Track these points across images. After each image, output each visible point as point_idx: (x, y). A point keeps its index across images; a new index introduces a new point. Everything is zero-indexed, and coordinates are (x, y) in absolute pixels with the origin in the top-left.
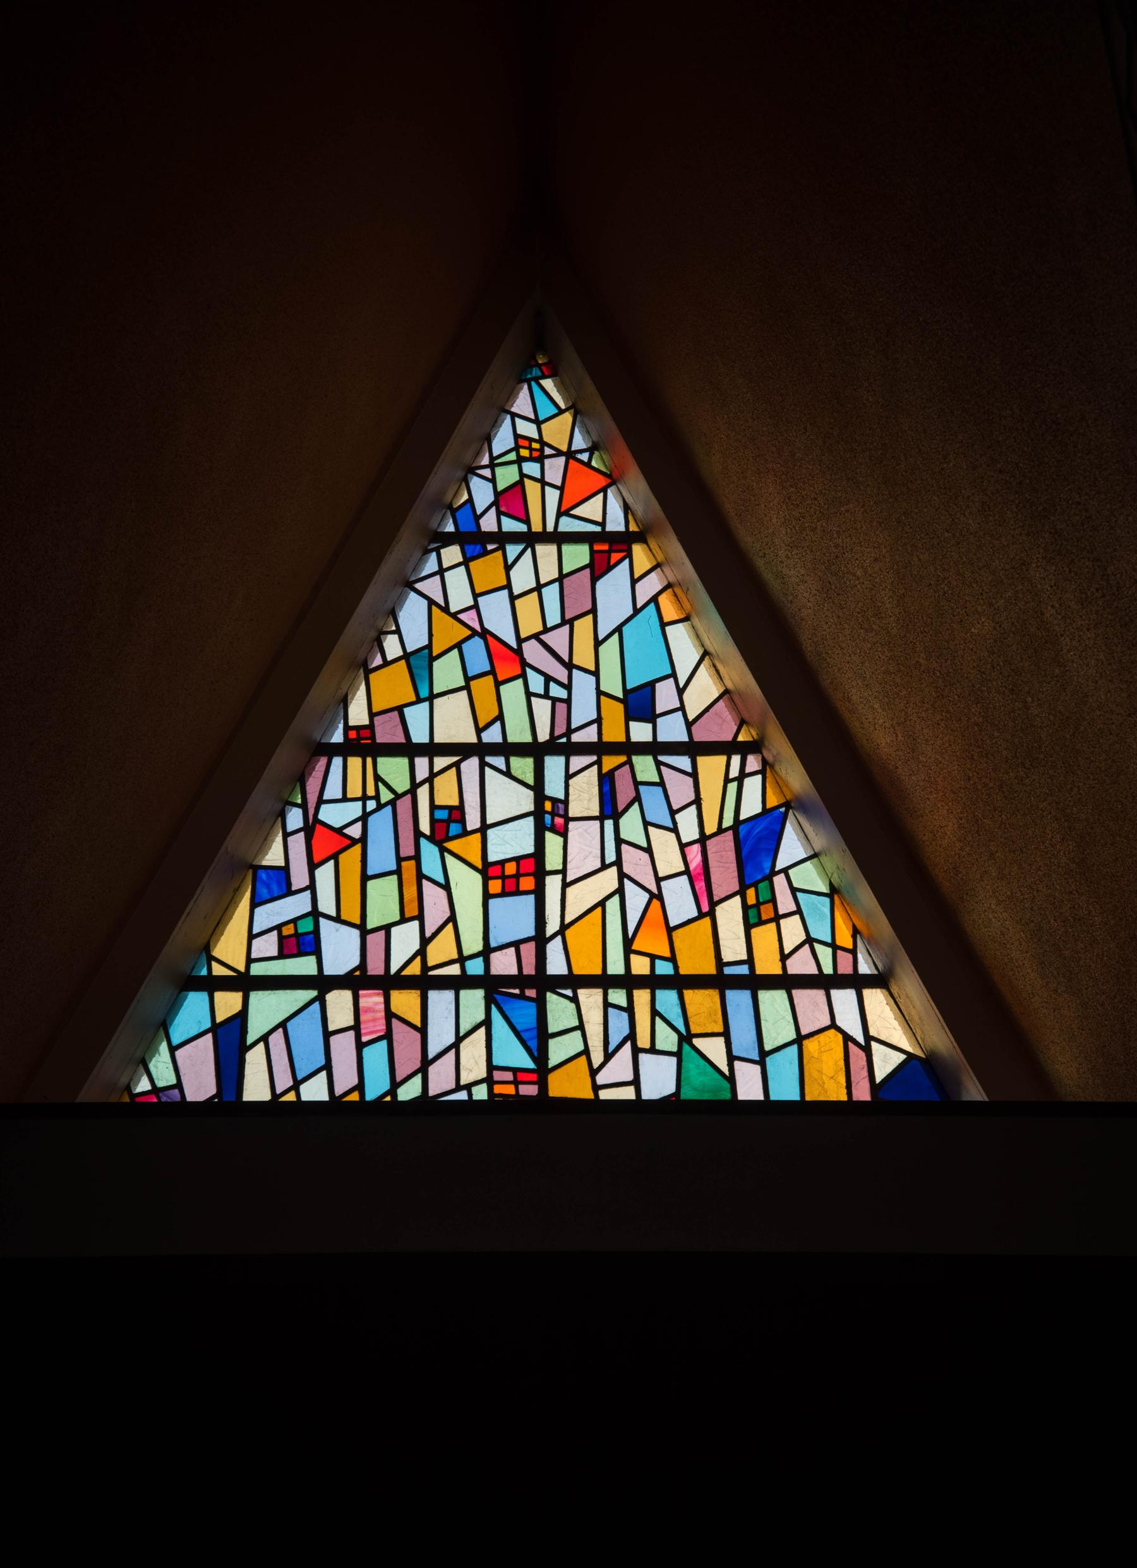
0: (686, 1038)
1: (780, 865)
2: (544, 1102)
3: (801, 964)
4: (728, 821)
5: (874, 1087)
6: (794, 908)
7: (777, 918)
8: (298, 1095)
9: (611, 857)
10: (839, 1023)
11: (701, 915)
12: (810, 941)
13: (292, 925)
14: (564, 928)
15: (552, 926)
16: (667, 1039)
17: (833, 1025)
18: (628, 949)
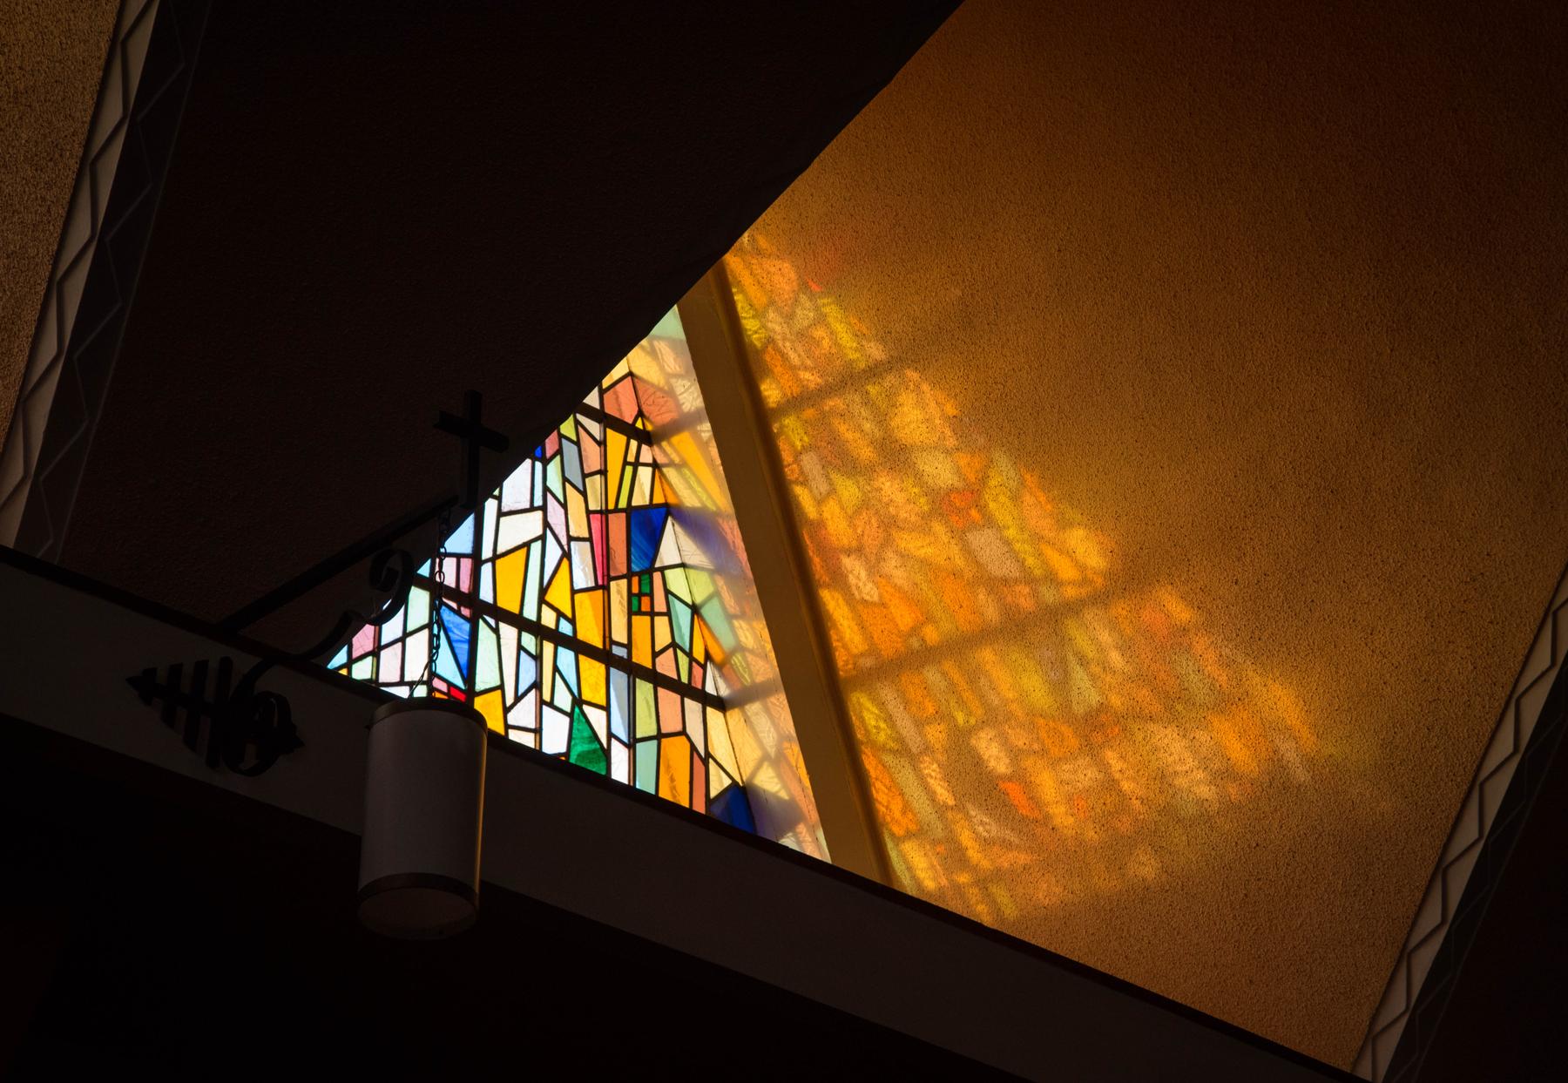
0: (578, 701)
1: (657, 565)
2: (567, 762)
3: (665, 666)
4: (623, 504)
5: (709, 802)
6: (665, 610)
7: (652, 614)
8: (350, 672)
9: (538, 502)
10: (689, 731)
11: (596, 588)
12: (674, 645)
13: (664, 609)
14: (495, 557)
15: (487, 552)
16: (564, 700)
17: (683, 733)
18: (542, 600)
